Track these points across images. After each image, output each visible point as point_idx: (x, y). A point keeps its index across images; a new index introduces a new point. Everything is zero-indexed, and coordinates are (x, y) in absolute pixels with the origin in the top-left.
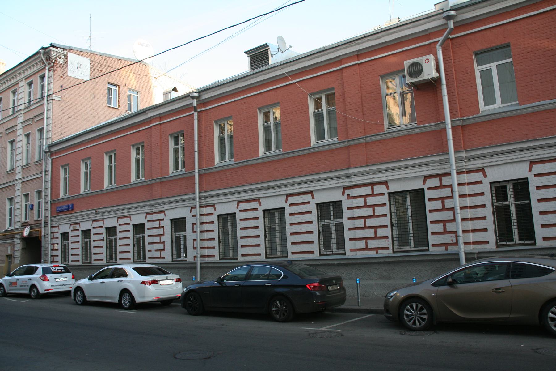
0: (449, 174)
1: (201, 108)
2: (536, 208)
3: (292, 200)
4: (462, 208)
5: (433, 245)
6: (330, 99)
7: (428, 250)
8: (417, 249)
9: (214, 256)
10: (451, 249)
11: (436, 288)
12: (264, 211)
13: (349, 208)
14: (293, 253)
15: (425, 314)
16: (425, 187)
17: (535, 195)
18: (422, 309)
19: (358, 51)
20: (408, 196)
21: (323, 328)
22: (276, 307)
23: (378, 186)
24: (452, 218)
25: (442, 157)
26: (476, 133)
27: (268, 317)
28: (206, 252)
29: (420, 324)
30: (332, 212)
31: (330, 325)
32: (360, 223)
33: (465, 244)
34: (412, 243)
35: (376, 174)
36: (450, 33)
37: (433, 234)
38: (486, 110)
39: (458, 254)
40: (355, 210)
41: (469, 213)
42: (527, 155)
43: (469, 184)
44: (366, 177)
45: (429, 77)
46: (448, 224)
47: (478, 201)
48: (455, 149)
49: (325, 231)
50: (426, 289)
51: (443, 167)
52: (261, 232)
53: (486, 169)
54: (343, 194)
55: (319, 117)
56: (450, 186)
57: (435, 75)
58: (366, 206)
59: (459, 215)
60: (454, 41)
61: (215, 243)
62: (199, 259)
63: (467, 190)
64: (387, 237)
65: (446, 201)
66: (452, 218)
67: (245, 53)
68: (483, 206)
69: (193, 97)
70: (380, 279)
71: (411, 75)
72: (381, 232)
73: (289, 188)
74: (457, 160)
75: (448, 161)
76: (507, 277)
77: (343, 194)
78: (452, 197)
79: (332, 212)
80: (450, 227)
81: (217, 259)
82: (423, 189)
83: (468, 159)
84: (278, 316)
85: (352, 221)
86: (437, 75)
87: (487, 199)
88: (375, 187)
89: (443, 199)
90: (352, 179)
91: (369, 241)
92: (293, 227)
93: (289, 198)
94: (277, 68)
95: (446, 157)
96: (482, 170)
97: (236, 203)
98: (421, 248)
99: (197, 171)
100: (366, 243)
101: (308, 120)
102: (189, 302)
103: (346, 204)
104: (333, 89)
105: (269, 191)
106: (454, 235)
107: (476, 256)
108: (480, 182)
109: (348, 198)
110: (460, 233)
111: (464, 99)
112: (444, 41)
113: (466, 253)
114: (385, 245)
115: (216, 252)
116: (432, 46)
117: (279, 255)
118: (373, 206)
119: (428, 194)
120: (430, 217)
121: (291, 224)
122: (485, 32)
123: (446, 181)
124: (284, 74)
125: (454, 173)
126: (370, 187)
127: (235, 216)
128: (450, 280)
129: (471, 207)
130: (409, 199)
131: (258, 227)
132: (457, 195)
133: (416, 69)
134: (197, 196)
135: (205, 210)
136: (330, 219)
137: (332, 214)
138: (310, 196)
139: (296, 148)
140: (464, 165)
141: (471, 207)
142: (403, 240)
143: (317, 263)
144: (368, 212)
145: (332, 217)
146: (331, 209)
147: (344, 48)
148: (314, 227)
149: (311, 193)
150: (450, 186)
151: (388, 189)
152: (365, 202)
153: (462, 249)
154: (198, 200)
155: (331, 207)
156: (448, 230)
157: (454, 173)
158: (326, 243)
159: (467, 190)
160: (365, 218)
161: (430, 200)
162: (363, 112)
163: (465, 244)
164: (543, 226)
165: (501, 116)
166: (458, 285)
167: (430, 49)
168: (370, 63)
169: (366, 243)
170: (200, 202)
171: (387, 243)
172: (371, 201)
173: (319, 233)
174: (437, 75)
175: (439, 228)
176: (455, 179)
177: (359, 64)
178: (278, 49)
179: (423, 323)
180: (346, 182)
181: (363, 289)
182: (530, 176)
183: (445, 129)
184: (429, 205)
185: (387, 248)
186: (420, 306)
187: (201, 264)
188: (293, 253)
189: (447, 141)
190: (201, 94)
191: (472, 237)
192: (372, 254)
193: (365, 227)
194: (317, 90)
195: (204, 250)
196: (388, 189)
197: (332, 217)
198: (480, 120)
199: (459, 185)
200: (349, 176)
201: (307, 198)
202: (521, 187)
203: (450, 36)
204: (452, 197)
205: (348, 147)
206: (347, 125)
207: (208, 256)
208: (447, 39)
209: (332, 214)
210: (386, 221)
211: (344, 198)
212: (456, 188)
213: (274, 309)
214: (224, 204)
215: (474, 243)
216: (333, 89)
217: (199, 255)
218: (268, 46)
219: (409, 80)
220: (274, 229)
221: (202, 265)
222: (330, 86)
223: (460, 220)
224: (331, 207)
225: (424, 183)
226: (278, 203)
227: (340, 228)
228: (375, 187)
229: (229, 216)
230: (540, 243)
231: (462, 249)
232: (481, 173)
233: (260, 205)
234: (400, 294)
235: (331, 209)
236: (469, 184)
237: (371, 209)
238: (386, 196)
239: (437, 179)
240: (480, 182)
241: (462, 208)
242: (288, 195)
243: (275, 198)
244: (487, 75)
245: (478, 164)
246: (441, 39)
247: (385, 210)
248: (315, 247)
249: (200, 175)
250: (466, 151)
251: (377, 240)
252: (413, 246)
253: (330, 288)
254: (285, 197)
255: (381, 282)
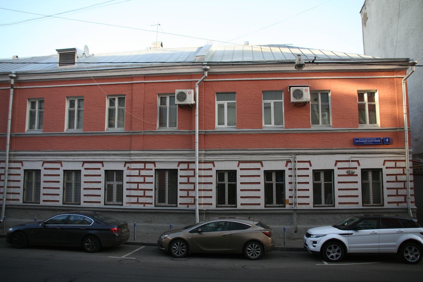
0: (194, 162)
1: (17, 86)
2: (239, 187)
3: (87, 165)
4: (199, 183)
5: (180, 204)
6: (121, 100)
7: (177, 206)
8: (170, 205)
9: (18, 200)
10: (191, 207)
11: (192, 234)
12: (64, 171)
13: (127, 176)
14: (85, 202)
15: (184, 248)
16: (179, 168)
17: (239, 180)
18: (183, 245)
19: (145, 74)
20: (167, 172)
21: (123, 257)
22: (88, 243)
23: (149, 164)
24: (193, 189)
25: (191, 152)
26: (212, 140)
27: (82, 249)
28: (11, 197)
29: (181, 254)
30: (115, 177)
31: (126, 254)
32: (135, 186)
33: (199, 204)
34: (167, 202)
35: (148, 156)
36: (204, 78)
37: (181, 197)
38: (219, 128)
39: (195, 210)
40: (132, 178)
41: (203, 187)
42: (238, 157)
43: (204, 169)
44: (141, 157)
45: (190, 103)
46: (190, 192)
47: (209, 180)
48: (199, 148)
49: (109, 189)
50: (185, 234)
51: (191, 158)
52: (61, 185)
53: (215, 162)
54: (125, 166)
55: (111, 112)
56: (194, 170)
57: (193, 102)
58: (139, 176)
59: (198, 187)
60: (206, 83)
61: (21, 191)
62: (5, 202)
63: (203, 173)
64: (152, 197)
65: (190, 178)
66: (193, 189)
67: (57, 50)
68: (211, 183)
69: (12, 77)
70: (145, 222)
71: (178, 99)
72: (148, 193)
73: (85, 157)
74: (200, 154)
75: (194, 155)
76: (229, 229)
77: (125, 166)
78: (194, 176)
79: (115, 177)
80: (191, 194)
81: (21, 202)
82: (177, 169)
83: (206, 155)
84: (89, 249)
85: (129, 184)
86: (194, 102)
87: (214, 180)
88: (146, 164)
89: (188, 177)
90: (132, 158)
91: (139, 198)
92: (86, 184)
93: (85, 164)
94: (85, 72)
95: (193, 152)
96: (212, 162)
97: (42, 162)
98: (172, 205)
99: (9, 134)
100: (138, 199)
101: (104, 113)
102: (15, 239)
103: (126, 172)
104: (125, 95)
105: (70, 157)
106: (193, 199)
107: (204, 212)
108: (211, 169)
109: (128, 169)
110: (197, 198)
111: (207, 120)
112: (200, 82)
113: (199, 210)
114: (150, 202)
115: (20, 197)
116: (193, 83)
117: (73, 203)
118: (144, 176)
119: (180, 173)
120: (180, 187)
121: (85, 182)
122: (224, 83)
123: (191, 166)
124: (91, 77)
125: (197, 162)
126: (143, 164)
127: (40, 172)
128: (200, 230)
129: (204, 183)
130: (167, 174)
131: (58, 182)
132: (197, 176)
133: (182, 96)
134: (8, 154)
135: (13, 165)
136: (114, 181)
137: (115, 178)
138: (101, 164)
139: (94, 131)
140: (203, 158)
141: (204, 183)
142: (161, 198)
143: (103, 210)
144: (141, 180)
145: (115, 180)
146: (115, 175)
147: (136, 71)
148: (102, 186)
149: (102, 162)
150: (194, 170)
151: (155, 166)
152: (139, 173)
153: (198, 208)
154: (8, 156)
155: (115, 173)
156: (190, 195)
157: (197, 162)
158: (109, 198)
159: (203, 173)
160: (138, 183)
161: (181, 176)
162: (144, 115)
163: (199, 204)
164: (241, 197)
165: (227, 133)
166: (203, 233)
167: (191, 86)
168: (152, 84)
169: (138, 199)
170: (9, 158)
171: (152, 200)
172: (143, 173)
173: (105, 190)
174: (194, 102)
175: (185, 194)
176: (197, 166)
177: (144, 83)
178: (83, 54)
179: (183, 253)
180: (127, 159)
181: (141, 230)
182: (238, 169)
183: (194, 135)
184: (180, 180)
185: (151, 204)
186: (182, 244)
187: (6, 205)
188: (85, 202)
189: (195, 143)
190: (18, 75)
191: (203, 201)
192: (141, 206)
193: (138, 189)
194: (113, 94)
195: (9, 195)
196: (155, 166)
197: (115, 180)
198: (215, 133)
199: (199, 169)
200: (130, 155)
201: (99, 165)
202: (232, 174)
203: (204, 80)
204: (194, 176)
205: (131, 136)
206: (132, 122)
207: (13, 200)
208: (203, 81)
209: (115, 178)
210: (152, 186)
211: (125, 169)
212: (197, 171)
213: (86, 244)
214: (30, 162)
215: (204, 204)
216: (125, 95)
217: (5, 199)
218: (76, 50)
219: (177, 102)
220: (71, 184)
221: (7, 207)
222: (123, 93)
223: (198, 191)
224: (115, 173)
225: (178, 166)
226: (77, 166)
227: (120, 188)
228: (146, 164)
229: (34, 171)
230: (239, 207)
231: (198, 208)
232: (212, 164)
233: (62, 166)
234: (170, 237)
235: (115, 175)
236: (204, 169)
237: (143, 178)
238: (154, 171)
239: (186, 165)
240: (211, 169)
241: (199, 183)
242: (84, 162)
243: (74, 163)
244: (221, 107)
245: (211, 158)
246: (200, 80)
247: (152, 180)
248: (102, 199)
249: (11, 138)
250: (205, 150)
251: (145, 198)
252: (167, 203)
253: (123, 231)
254: (82, 163)
255: (146, 224)
